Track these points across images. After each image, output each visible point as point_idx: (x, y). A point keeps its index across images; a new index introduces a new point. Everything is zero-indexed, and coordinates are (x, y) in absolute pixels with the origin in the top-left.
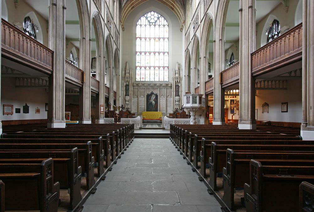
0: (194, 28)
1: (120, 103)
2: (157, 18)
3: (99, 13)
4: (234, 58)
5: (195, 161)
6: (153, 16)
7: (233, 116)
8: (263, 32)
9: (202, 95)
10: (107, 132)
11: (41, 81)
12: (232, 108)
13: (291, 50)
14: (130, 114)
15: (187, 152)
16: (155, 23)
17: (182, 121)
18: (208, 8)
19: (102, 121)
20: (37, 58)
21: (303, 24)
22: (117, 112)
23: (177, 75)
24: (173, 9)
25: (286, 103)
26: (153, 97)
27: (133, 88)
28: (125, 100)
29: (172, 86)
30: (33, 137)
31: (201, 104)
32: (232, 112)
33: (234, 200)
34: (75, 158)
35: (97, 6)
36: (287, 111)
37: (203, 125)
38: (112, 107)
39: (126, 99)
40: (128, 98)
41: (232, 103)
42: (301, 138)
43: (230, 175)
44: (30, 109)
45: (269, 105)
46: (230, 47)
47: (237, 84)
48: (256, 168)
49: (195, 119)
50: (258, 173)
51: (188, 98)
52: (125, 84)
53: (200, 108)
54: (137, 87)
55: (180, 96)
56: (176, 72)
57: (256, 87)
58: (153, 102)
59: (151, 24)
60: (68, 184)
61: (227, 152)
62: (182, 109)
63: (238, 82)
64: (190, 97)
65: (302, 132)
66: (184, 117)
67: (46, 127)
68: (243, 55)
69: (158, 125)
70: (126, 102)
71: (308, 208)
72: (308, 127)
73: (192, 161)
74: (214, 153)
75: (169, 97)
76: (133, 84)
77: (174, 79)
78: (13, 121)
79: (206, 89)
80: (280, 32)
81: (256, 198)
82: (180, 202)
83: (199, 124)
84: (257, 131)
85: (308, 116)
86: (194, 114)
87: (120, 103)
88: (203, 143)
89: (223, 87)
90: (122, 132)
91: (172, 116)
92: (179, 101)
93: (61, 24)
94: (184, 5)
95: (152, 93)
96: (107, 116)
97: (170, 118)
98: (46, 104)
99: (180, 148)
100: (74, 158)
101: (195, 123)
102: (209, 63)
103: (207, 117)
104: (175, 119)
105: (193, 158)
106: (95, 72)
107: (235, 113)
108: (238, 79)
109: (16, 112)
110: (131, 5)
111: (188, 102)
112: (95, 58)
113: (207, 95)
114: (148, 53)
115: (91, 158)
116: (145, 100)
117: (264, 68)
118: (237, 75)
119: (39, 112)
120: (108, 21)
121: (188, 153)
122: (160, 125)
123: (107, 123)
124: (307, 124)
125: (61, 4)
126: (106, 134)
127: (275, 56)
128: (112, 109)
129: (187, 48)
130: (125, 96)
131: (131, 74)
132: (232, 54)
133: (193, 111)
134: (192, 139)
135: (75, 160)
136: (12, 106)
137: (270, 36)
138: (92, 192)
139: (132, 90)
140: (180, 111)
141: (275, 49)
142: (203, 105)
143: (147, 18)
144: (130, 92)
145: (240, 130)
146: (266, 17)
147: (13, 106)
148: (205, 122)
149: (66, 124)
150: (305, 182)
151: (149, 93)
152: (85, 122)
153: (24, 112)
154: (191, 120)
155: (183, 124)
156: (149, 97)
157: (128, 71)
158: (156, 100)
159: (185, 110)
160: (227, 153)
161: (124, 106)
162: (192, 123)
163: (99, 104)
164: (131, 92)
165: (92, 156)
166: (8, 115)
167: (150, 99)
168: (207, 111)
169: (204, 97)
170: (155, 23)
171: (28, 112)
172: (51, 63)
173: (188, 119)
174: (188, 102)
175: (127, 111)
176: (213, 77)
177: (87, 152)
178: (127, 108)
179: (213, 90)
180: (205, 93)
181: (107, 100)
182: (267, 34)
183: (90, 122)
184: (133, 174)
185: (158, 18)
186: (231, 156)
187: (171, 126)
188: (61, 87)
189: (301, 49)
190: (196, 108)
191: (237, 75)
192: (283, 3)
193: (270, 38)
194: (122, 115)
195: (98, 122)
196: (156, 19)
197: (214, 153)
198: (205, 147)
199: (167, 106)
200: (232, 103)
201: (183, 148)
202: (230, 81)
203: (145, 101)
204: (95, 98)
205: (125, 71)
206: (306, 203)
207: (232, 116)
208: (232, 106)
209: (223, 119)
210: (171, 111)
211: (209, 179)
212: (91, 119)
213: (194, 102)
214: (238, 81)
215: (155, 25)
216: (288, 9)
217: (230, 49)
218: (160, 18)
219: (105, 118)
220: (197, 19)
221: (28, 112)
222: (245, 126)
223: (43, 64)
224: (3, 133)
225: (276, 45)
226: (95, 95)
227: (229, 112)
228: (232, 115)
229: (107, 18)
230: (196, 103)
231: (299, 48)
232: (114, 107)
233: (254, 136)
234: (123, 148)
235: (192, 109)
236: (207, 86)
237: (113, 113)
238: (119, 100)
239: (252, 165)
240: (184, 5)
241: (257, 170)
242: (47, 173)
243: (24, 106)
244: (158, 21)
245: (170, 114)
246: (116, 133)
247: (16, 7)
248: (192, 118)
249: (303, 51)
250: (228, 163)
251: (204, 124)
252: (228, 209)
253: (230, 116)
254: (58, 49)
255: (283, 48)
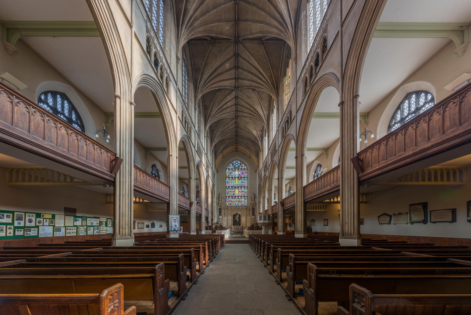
0: (264, 170)
1: (215, 221)
2: (239, 164)
3: (201, 161)
4: (291, 190)
5: (266, 260)
6: (237, 163)
7: (291, 228)
8: (311, 173)
9: (270, 215)
10: (209, 239)
11: (162, 206)
12: (290, 223)
13: (332, 184)
14: (222, 228)
15: (260, 253)
16: (238, 167)
17: (256, 232)
18: (304, 99)
19: (203, 232)
20: (159, 191)
21: (341, 166)
22: (214, 226)
23: (253, 202)
24: (250, 158)
25: (326, 220)
26: (237, 216)
27: (224, 211)
28: (219, 218)
29: (249, 209)
30: (155, 245)
31: (269, 220)
32: (290, 225)
33: (295, 289)
34: (181, 261)
35: (198, 154)
36: (327, 225)
37: (270, 235)
38: (210, 223)
39: (220, 218)
40: (220, 217)
41: (290, 220)
42: (340, 244)
43: (292, 272)
44: (156, 225)
45: (315, 221)
46: (289, 183)
47: (294, 207)
48: (312, 270)
49: (265, 231)
50: (314, 273)
51: (260, 217)
52: (219, 208)
53: (269, 224)
54: (227, 210)
55: (255, 215)
56: (253, 199)
57: (75, 235)
58: (238, 220)
59: (236, 168)
60: (190, 267)
61: (289, 256)
62: (257, 224)
63: (295, 206)
64: (262, 216)
65: (340, 240)
66: (258, 230)
67: (165, 237)
68: (298, 188)
69: (241, 234)
70: (220, 220)
71: (357, 304)
72: (344, 236)
73: (264, 260)
74: (279, 256)
75: (248, 216)
76: (224, 208)
77: (251, 204)
78: (153, 232)
79: (273, 210)
80: (322, 172)
81: (313, 291)
82: (256, 291)
83: (268, 234)
84: (308, 239)
85: (344, 229)
86: (265, 227)
87: (216, 220)
88: (271, 248)
89: (284, 209)
90: (216, 240)
91: (250, 229)
92: (255, 218)
93: (175, 168)
94: (257, 155)
95: (237, 214)
96: (207, 229)
97: (248, 230)
98: (166, 222)
99: (256, 251)
100: (181, 261)
101: (266, 233)
102: (275, 194)
103: (273, 229)
104: (252, 231)
105: (264, 258)
106: (199, 200)
107: (292, 226)
108: (295, 204)
109: (146, 227)
110: (223, 156)
111: (260, 220)
112: (199, 191)
113: (273, 215)
114: (237, 197)
115: (194, 260)
116: (232, 218)
117: (313, 196)
118: (294, 201)
119: (162, 227)
120: (207, 166)
121: (261, 254)
122: (242, 234)
123: (207, 234)
124: (343, 234)
125: (175, 155)
126: (209, 241)
127: (320, 188)
128: (210, 224)
129: (260, 184)
130: (219, 216)
131: (223, 201)
132: (290, 187)
133: (264, 225)
134: (264, 245)
135: (182, 262)
136: (144, 223)
137: (316, 175)
138: (183, 298)
139: (223, 212)
140: (255, 226)
141: (320, 184)
142: (270, 221)
143: (233, 164)
144: (222, 213)
145: (296, 238)
146: (313, 162)
147: (144, 223)
148: (272, 232)
149: (179, 235)
150: (354, 284)
151: (235, 214)
152: (192, 233)
153: (152, 227)
154: (263, 231)
155: (257, 234)
156: (234, 216)
157: (221, 199)
158: (239, 218)
159: (259, 225)
160: (290, 257)
161: (218, 223)
162: (263, 234)
163: (201, 222)
164: (223, 213)
165: (195, 258)
166: (141, 229)
167: (236, 218)
168: (274, 225)
169: (271, 216)
170: (238, 167)
171: (154, 227)
172: (168, 195)
173: (261, 231)
174: (260, 220)
175: (220, 225)
176: (277, 202)
177: (190, 256)
178: (220, 224)
179: (277, 211)
180: (272, 213)
181: (207, 218)
182: (314, 173)
183: (195, 233)
184: (223, 269)
185: (241, 164)
186: (292, 259)
187: (250, 235)
188: (175, 210)
189: (339, 183)
190: (266, 223)
191: (294, 201)
192: (324, 153)
193: (315, 176)
194: (216, 228)
195: (201, 233)
196: (239, 165)
197: (279, 256)
198: (274, 251)
199: (246, 222)
200: (290, 220)
201: (258, 250)
202: (292, 204)
203: (232, 219)
204: (199, 218)
205: (219, 199)
206: (356, 300)
207: (290, 228)
208: (290, 222)
209: (284, 231)
210: (249, 225)
211: (276, 273)
212: (196, 231)
213: (265, 219)
214: (295, 205)
215: (238, 169)
216: (328, 156)
217: (288, 184)
218: (242, 164)
219: (205, 231)
220: (266, 164)
221: (154, 227)
222: (300, 235)
223: (163, 196)
224: (135, 242)
225: (318, 182)
226: (199, 216)
227: (288, 225)
228: (290, 227)
229: (207, 164)
230: (266, 220)
231: (333, 184)
232: (211, 223)
233: (374, 273)
234: (222, 246)
235: (263, 224)
236: (273, 208)
237: (211, 227)
238: (215, 218)
239: (309, 267)
240: (257, 155)
241: (313, 271)
242: (159, 274)
243: (151, 223)
244: (240, 166)
245: (249, 228)
246: (212, 241)
247: (146, 158)
248: (263, 230)
249: (341, 184)
250: (290, 264)
251: (271, 234)
252: (291, 296)
253: (289, 229)
254: (173, 185)
255: (326, 183)
